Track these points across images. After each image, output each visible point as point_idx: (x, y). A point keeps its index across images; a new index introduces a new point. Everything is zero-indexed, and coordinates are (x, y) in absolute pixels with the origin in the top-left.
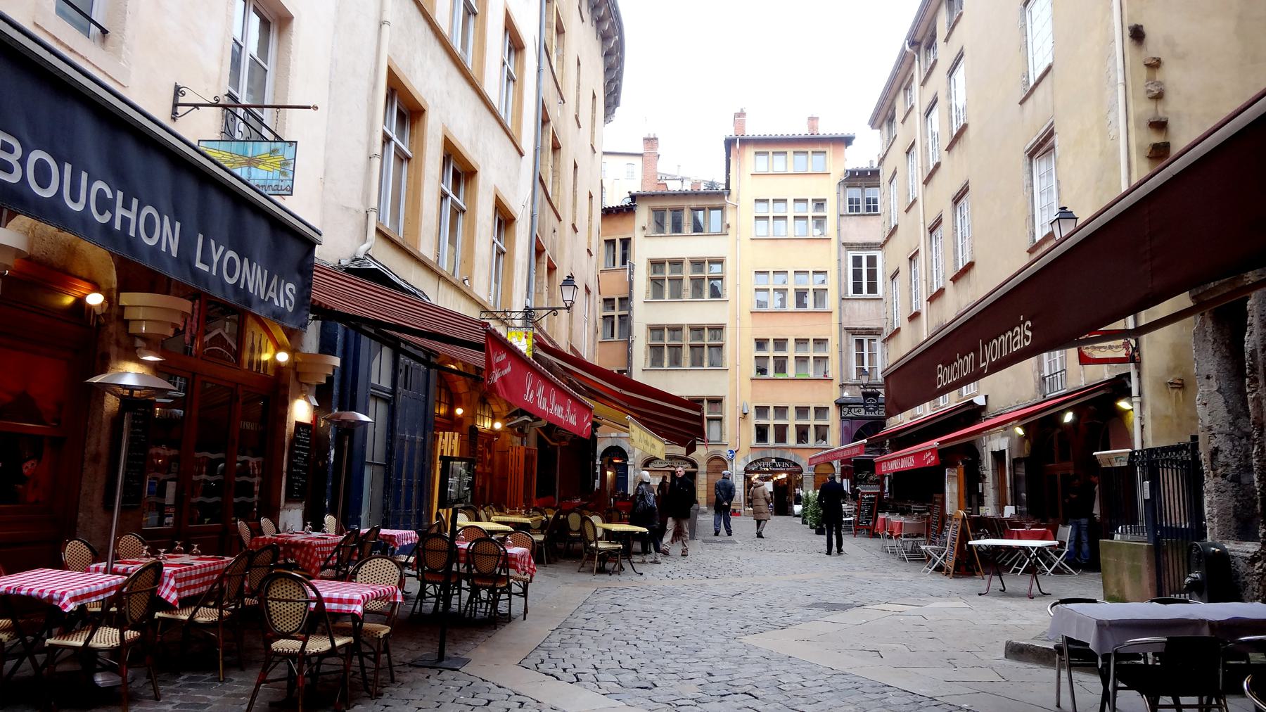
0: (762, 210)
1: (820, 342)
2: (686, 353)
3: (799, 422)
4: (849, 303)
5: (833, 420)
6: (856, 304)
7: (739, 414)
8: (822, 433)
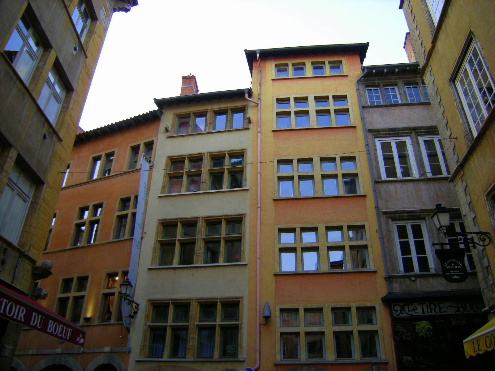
0: (286, 170)
1: (341, 98)
2: (200, 249)
3: (339, 328)
4: (385, 186)
5: (382, 323)
6: (392, 187)
7: (258, 319)
8: (369, 341)
